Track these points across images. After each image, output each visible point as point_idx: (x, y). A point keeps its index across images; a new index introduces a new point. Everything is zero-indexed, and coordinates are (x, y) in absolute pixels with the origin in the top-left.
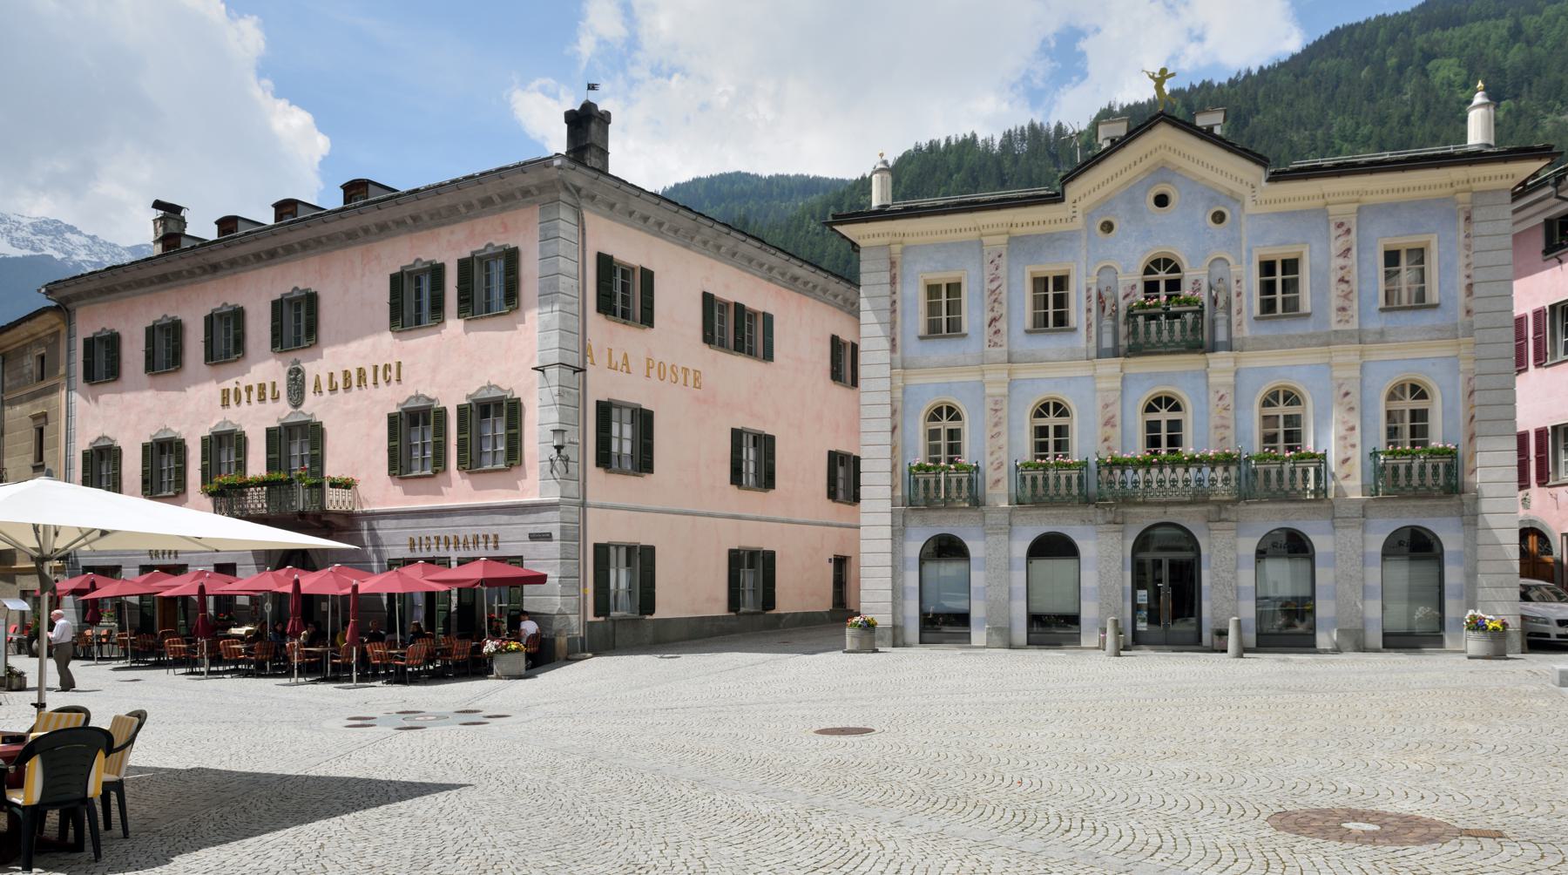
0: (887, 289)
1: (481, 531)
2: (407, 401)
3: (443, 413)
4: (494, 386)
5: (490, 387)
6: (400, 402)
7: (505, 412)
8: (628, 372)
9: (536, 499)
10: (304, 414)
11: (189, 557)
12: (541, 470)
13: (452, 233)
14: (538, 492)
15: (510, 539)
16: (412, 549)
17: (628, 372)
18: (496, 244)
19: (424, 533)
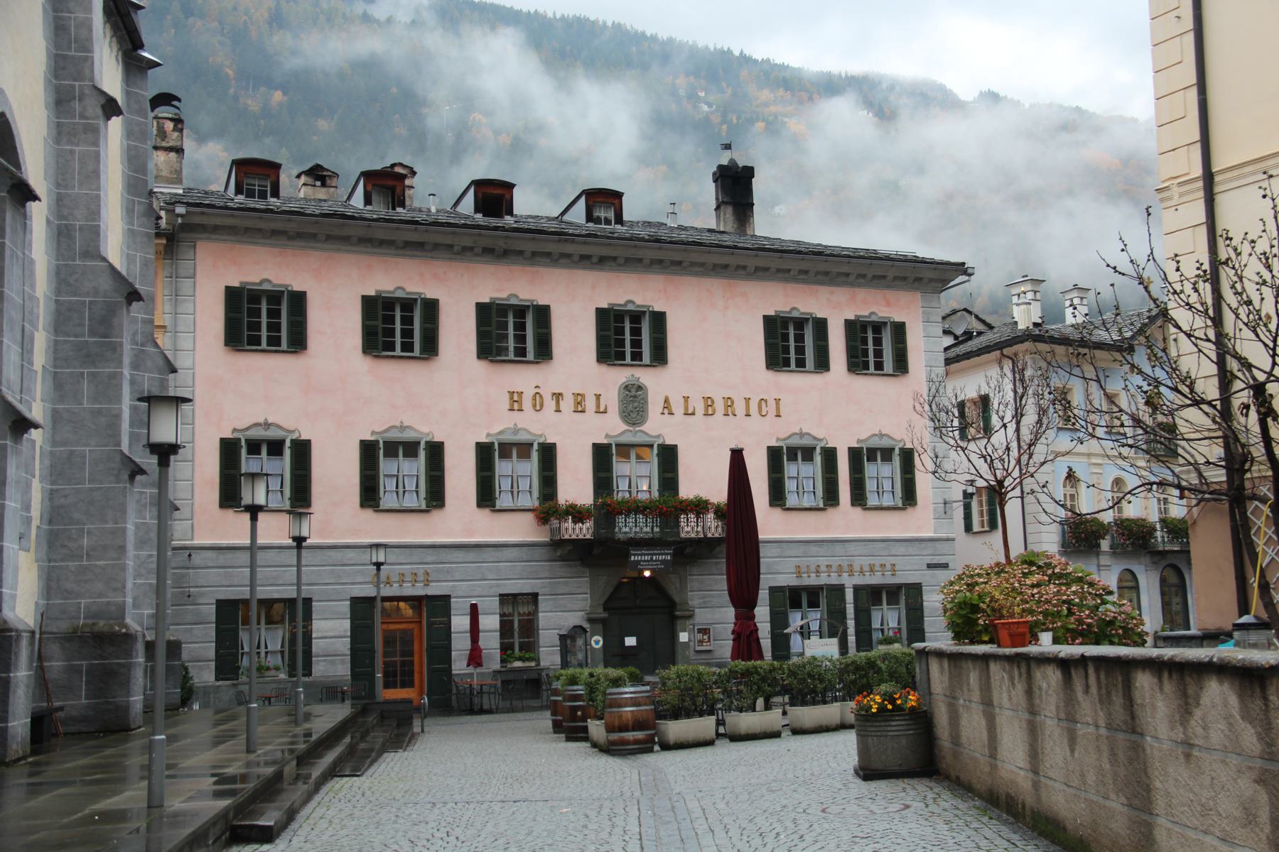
0: (304, 579)
1: (877, 561)
2: (789, 437)
3: (52, 490)
4: (884, 435)
5: (881, 435)
6: (378, 430)
7: (66, 564)
8: (671, 414)
9: (930, 534)
10: (645, 433)
11: (454, 586)
12: (935, 510)
13: (832, 293)
14: (933, 529)
15: (908, 568)
16: (799, 577)
17: (671, 414)
18: (880, 315)
19: (813, 562)
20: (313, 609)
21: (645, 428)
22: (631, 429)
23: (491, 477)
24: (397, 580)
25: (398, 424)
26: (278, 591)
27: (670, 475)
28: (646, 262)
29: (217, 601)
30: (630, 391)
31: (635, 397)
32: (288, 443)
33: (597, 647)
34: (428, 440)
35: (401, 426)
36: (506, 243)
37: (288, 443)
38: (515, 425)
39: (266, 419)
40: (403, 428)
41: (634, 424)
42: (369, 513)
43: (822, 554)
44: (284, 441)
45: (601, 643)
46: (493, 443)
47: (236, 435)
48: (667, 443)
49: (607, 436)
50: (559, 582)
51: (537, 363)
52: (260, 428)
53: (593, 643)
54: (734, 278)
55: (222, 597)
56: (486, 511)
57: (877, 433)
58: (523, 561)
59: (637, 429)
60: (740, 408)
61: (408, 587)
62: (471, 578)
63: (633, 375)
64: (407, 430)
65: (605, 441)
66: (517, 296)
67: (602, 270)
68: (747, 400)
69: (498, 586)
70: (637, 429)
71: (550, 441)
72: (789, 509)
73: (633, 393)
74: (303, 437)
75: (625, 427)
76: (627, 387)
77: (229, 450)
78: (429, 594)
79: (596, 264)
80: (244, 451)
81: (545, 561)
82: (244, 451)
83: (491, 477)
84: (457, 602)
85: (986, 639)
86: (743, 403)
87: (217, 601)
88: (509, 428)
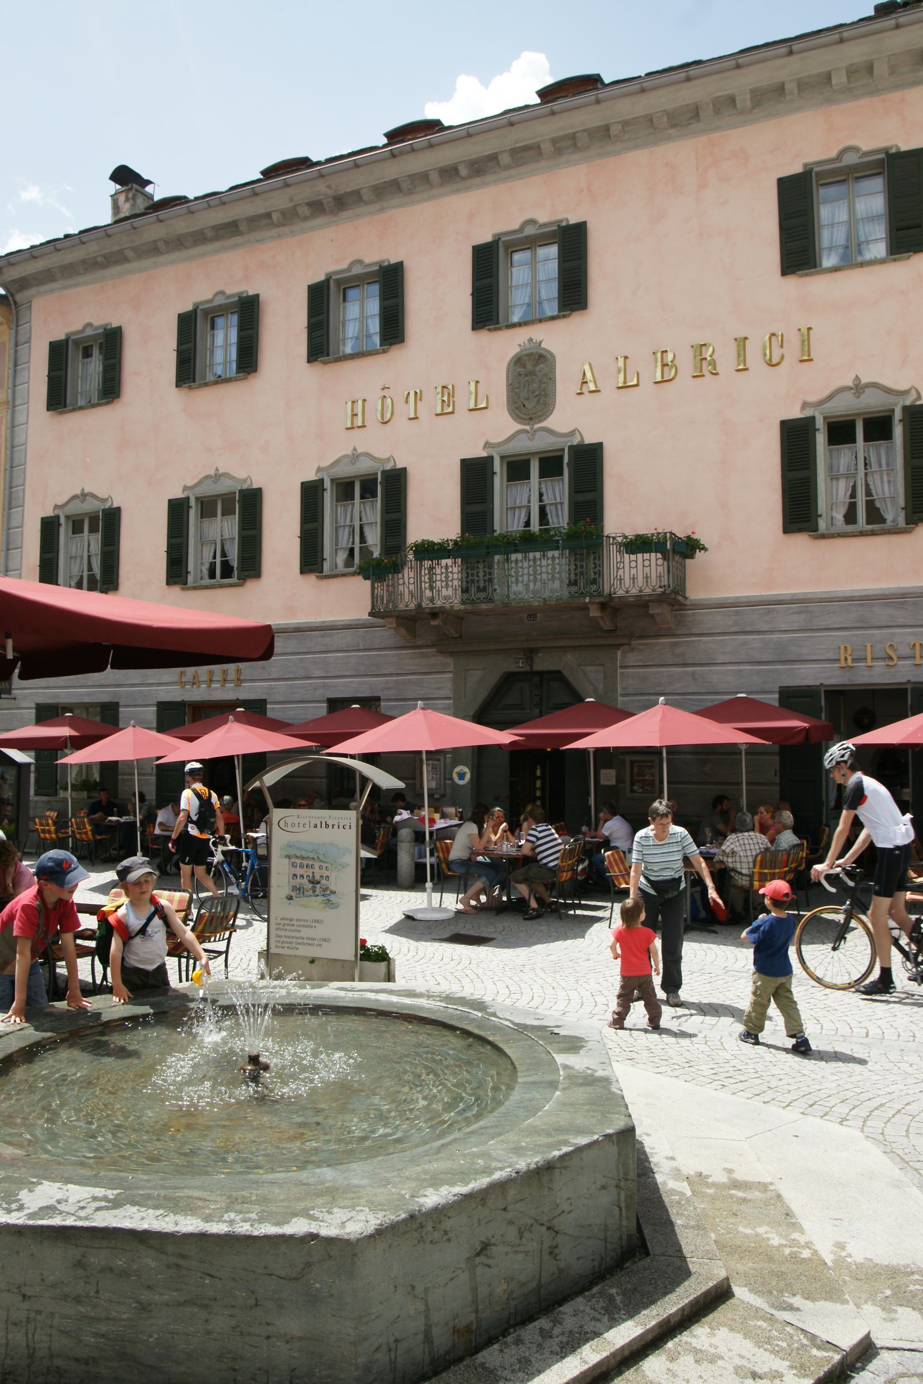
6: (189, 484)
11: (270, 688)
20: (120, 716)
21: (554, 422)
22: (527, 428)
23: (113, 552)
24: (219, 679)
25: (212, 473)
26: (88, 694)
27: (588, 496)
28: (744, 100)
29: (37, 704)
30: (524, 366)
31: (532, 373)
32: (898, 415)
33: (461, 783)
34: (908, 403)
35: (857, 386)
36: (329, 187)
37: (898, 415)
38: (355, 449)
39: (83, 490)
40: (218, 477)
41: (531, 419)
42: (801, 540)
43: (901, 621)
44: (893, 411)
45: (468, 777)
46: (812, 419)
47: (808, 413)
48: (586, 442)
49: (487, 445)
50: (409, 681)
51: (564, 317)
52: (78, 500)
53: (455, 776)
54: (718, 129)
55: (40, 700)
56: (312, 578)
57: (851, 384)
58: (359, 650)
59: (536, 426)
60: (726, 359)
61: (217, 689)
62: (291, 676)
63: (531, 340)
64: (222, 478)
65: (484, 454)
66: (360, 262)
67: (485, 185)
68: (742, 342)
69: (325, 686)
70: (536, 426)
71: (589, 439)
72: (823, 537)
73: (529, 367)
74: (399, 466)
75: (517, 427)
76: (518, 361)
77: (49, 527)
78: (241, 698)
79: (470, 177)
80: (821, 439)
81: (390, 648)
82: (821, 439)
83: (113, 552)
84: (273, 709)
85: (303, 802)
86: (732, 349)
87: (37, 704)
88: (346, 456)
